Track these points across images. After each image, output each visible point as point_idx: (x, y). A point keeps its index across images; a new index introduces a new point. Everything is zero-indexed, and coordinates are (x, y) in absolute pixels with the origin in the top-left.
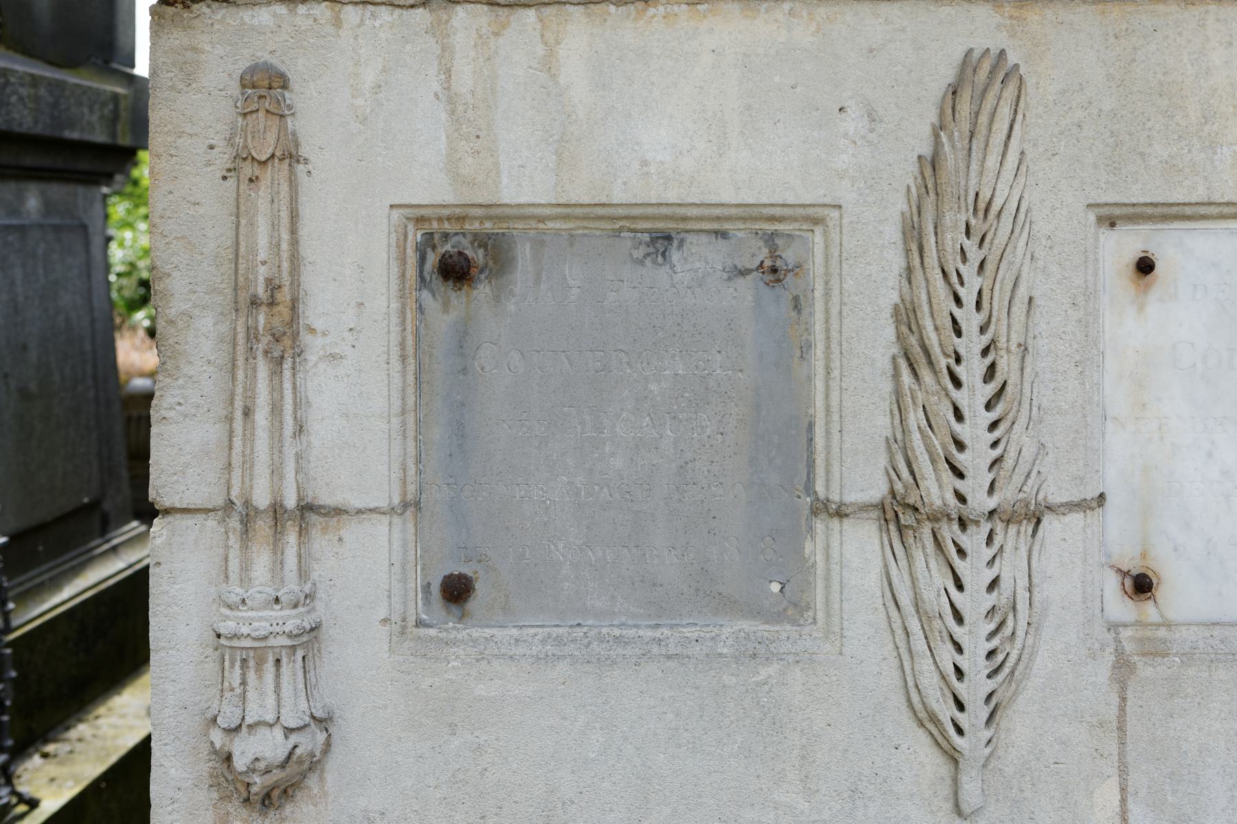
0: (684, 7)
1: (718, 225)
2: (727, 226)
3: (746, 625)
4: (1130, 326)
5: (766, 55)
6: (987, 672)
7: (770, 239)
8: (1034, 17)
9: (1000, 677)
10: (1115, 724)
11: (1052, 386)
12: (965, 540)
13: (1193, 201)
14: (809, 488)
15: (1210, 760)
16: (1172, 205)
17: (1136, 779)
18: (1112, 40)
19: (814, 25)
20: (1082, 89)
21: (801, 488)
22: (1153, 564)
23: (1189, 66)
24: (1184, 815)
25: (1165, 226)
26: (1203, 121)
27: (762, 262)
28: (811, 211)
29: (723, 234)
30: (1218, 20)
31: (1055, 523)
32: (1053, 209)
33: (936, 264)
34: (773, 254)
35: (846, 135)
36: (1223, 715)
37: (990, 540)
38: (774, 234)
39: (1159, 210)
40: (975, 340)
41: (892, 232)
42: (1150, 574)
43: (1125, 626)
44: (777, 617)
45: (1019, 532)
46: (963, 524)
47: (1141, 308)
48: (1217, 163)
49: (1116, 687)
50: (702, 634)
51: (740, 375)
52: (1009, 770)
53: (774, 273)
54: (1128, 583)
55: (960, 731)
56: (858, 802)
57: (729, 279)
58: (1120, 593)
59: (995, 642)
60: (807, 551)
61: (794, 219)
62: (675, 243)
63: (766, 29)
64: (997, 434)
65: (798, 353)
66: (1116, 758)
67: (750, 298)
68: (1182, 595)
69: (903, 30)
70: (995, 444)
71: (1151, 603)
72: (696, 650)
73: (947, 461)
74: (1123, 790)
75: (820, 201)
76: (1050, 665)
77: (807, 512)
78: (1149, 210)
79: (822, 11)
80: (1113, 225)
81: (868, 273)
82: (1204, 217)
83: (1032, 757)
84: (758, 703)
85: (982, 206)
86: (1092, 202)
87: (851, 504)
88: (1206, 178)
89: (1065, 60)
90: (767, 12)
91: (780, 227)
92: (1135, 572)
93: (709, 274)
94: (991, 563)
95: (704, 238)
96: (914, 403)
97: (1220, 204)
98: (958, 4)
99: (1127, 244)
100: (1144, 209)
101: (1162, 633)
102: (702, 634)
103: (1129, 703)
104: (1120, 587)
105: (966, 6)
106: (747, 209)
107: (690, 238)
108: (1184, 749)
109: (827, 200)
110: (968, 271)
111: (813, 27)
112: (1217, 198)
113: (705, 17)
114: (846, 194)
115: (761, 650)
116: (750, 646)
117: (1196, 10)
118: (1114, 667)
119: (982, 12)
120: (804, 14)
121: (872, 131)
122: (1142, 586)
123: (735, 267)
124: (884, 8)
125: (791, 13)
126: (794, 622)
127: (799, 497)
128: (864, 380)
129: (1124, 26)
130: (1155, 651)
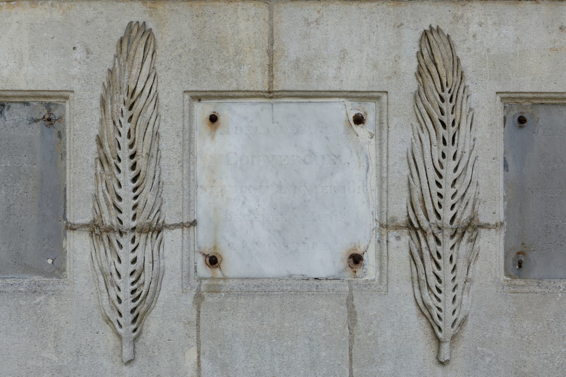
0: (5, 3)
1: (25, 99)
2: (27, 100)
3: (36, 278)
4: (207, 146)
5: (41, 24)
6: (131, 299)
7: (48, 106)
8: (161, 8)
9: (137, 302)
10: (195, 323)
11: (168, 172)
12: (122, 241)
13: (231, 90)
14: (65, 218)
15: (237, 339)
16: (222, 91)
17: (204, 347)
18: (195, 18)
19: (62, 10)
20: (181, 40)
21: (61, 217)
22: (218, 252)
23: (229, 29)
24: (226, 363)
25: (223, 101)
26: (235, 54)
27: (44, 116)
28: (61, 93)
29: (27, 104)
30: (243, 9)
31: (169, 233)
32: (168, 93)
33: (110, 117)
34: (49, 113)
35: (76, 59)
36: (243, 319)
37: (133, 241)
38: (50, 103)
39: (217, 94)
40: (126, 151)
41: (96, 103)
42: (217, 256)
43: (206, 279)
44: (50, 275)
45: (147, 237)
46: (121, 233)
47: (213, 138)
48: (241, 73)
49: (196, 306)
50: (15, 282)
51: (34, 166)
52: (148, 343)
53: (49, 121)
54: (208, 260)
55: (120, 326)
56: (80, 358)
57: (30, 123)
58: (204, 264)
59: (135, 286)
60: (64, 245)
61: (56, 97)
62: (6, 107)
63: (41, 13)
64: (136, 193)
65: (60, 157)
66: (195, 338)
67: (39, 132)
68: (233, 266)
69: (102, 13)
70: (136, 198)
71: (218, 269)
72: (9, 289)
73: (114, 205)
74: (199, 352)
75: (64, 89)
76: (166, 296)
77: (64, 228)
78: (213, 94)
79: (66, 4)
80: (200, 100)
81: (85, 121)
82: (238, 97)
83: (158, 337)
84: (36, 313)
85: (130, 92)
86: (186, 90)
87: (78, 224)
88: (237, 80)
89: (174, 28)
90: (41, 5)
91: (51, 100)
92: (210, 255)
93: (21, 121)
94: (134, 250)
95: (19, 105)
96: (102, 180)
97: (244, 91)
98: (126, 1)
99: (203, 110)
100: (210, 93)
101: (221, 282)
102: (15, 282)
103: (201, 313)
104: (204, 262)
105: (130, 2)
106: (33, 93)
107: (13, 105)
108: (226, 334)
109: (67, 89)
110: (124, 120)
111: (61, 12)
112: (241, 88)
113: (14, 7)
114: (76, 86)
115: (39, 289)
116: (34, 287)
117: (233, 5)
118: (195, 298)
119: (137, 5)
120: (58, 5)
121: (88, 58)
122: (213, 261)
123: (32, 118)
124: (93, 4)
125: (52, 5)
126: (58, 277)
127: (60, 221)
128: (83, 169)
129: (201, 12)
130: (214, 290)
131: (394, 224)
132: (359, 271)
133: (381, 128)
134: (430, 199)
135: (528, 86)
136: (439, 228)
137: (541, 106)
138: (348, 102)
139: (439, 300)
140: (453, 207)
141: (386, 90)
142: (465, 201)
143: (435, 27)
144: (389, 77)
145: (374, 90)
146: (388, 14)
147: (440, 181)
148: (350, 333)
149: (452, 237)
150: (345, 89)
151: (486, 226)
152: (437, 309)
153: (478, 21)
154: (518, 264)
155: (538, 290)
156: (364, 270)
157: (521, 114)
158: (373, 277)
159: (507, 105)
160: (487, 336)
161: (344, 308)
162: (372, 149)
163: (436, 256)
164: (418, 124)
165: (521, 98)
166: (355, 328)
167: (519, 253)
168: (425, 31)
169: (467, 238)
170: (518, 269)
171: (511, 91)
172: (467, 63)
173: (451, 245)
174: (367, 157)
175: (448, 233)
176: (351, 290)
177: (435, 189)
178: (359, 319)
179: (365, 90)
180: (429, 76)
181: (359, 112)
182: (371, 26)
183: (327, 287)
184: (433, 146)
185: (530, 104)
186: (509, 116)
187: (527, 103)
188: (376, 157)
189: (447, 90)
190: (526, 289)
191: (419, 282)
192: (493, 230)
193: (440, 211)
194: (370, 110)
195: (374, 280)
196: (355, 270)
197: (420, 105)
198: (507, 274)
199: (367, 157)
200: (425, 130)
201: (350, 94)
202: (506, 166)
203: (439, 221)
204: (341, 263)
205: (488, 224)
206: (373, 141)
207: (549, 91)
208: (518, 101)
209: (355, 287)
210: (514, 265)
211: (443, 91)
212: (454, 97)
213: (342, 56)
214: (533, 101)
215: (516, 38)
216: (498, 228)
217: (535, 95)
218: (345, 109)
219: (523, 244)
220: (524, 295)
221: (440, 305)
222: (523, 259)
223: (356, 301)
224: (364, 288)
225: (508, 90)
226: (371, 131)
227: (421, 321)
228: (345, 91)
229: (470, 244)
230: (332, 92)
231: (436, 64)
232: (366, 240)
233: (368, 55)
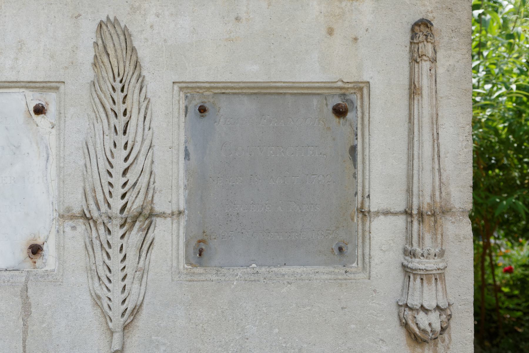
131: (70, 214)
132: (39, 262)
133: (60, 118)
134: (100, 188)
135: (203, 75)
136: (110, 218)
137: (222, 95)
138: (27, 92)
139: (109, 290)
140: (123, 196)
141: (63, 81)
142: (136, 189)
143: (112, 18)
144: (66, 67)
145: (51, 80)
146: (66, 5)
147: (111, 170)
148: (24, 325)
149: (122, 226)
150: (22, 80)
151: (162, 215)
152: (107, 299)
153: (155, 12)
154: (199, 252)
155: (214, 278)
156: (44, 261)
157: (202, 105)
158: (53, 268)
159: (189, 95)
160: (162, 325)
161: (18, 299)
162: (52, 140)
163: (106, 246)
164: (94, 114)
165: (200, 88)
166: (29, 319)
167: (200, 242)
168: (101, 21)
169: (138, 227)
170: (199, 258)
171: (187, 81)
172: (144, 53)
173: (121, 235)
174: (47, 147)
175: (118, 222)
176: (27, 281)
177: (106, 178)
178: (33, 310)
179: (42, 80)
180: (103, 66)
181: (40, 102)
182: (48, 17)
183: (3, 278)
184: (105, 136)
185: (212, 93)
186: (190, 106)
187: (207, 93)
188: (57, 147)
189: (118, 79)
190: (203, 278)
191: (92, 272)
192: (169, 219)
193: (110, 200)
194: (50, 100)
195: (54, 271)
196: (34, 260)
197: (95, 95)
198: (188, 262)
199: (47, 147)
200: (99, 120)
201: (28, 85)
202: (187, 155)
203: (109, 211)
204: (22, 253)
205: (164, 213)
206: (54, 131)
207: (224, 81)
208: (198, 90)
209: (31, 278)
210: (195, 253)
211: (115, 81)
212: (126, 87)
213: (20, 47)
214: (212, 90)
215: (192, 28)
216: (174, 217)
217: (212, 85)
218: (22, 100)
219: (204, 232)
220: (199, 283)
221: (109, 295)
222: (203, 247)
223: (30, 292)
224: (40, 279)
225: (184, 80)
226: (53, 121)
227: (96, 311)
228: (23, 82)
229: (141, 233)
230: (9, 82)
231: (108, 55)
232: (44, 230)
233: (45, 45)
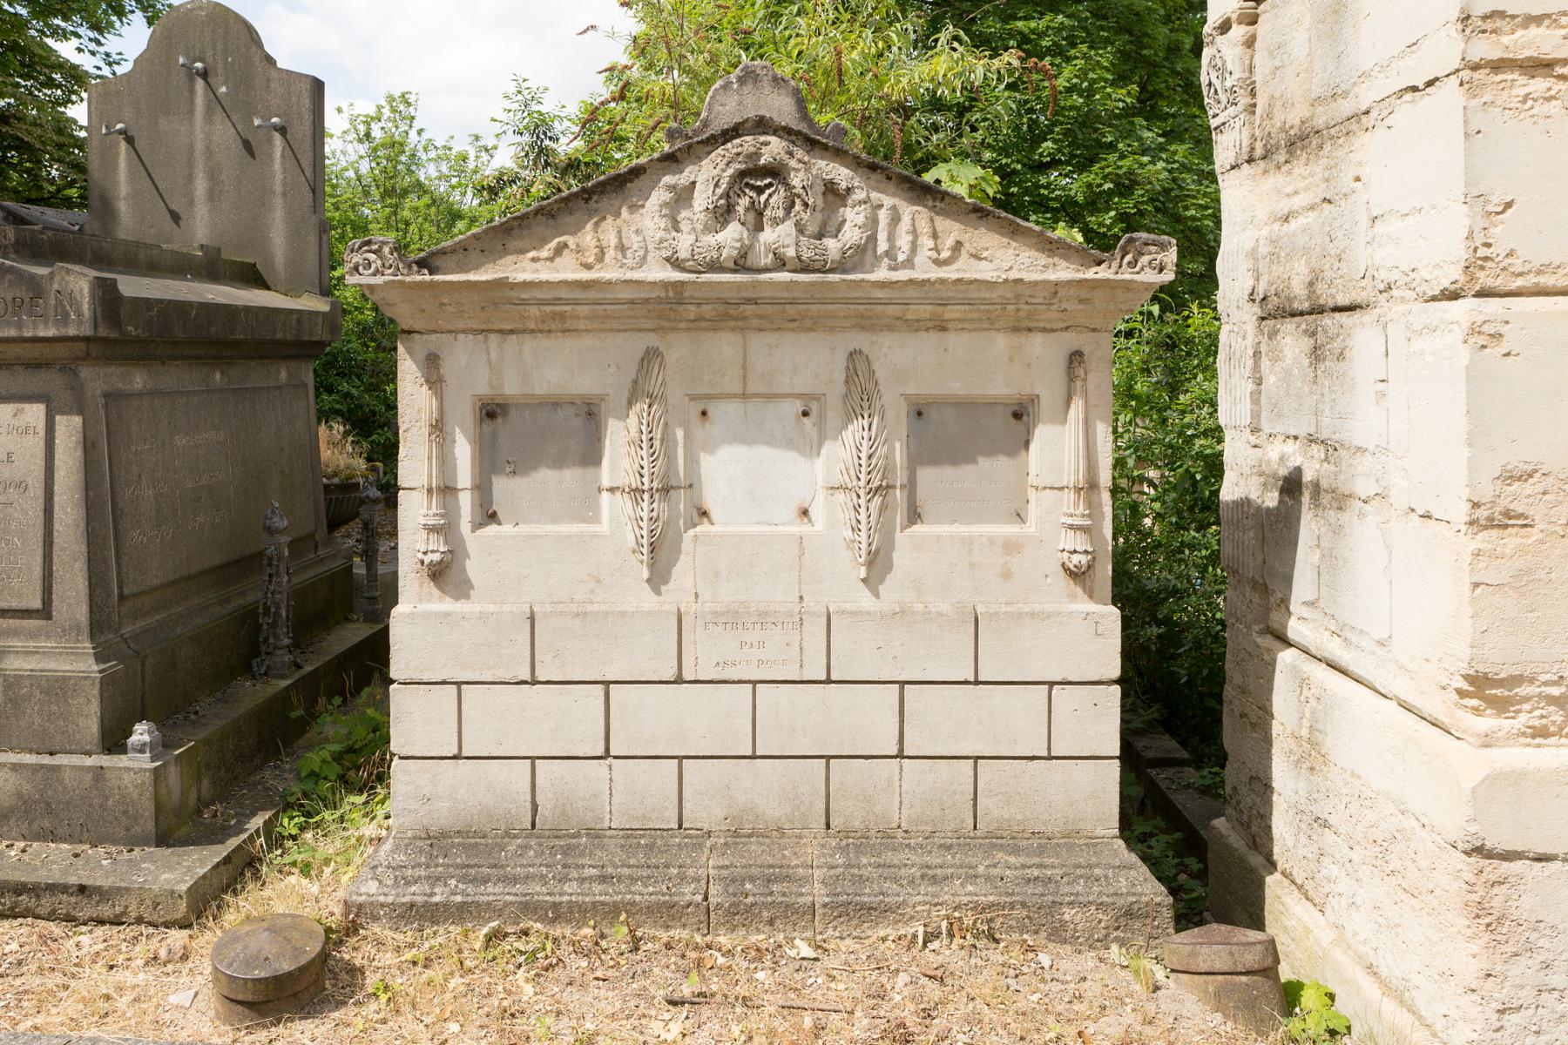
172: (880, 374)
218: (798, 406)
